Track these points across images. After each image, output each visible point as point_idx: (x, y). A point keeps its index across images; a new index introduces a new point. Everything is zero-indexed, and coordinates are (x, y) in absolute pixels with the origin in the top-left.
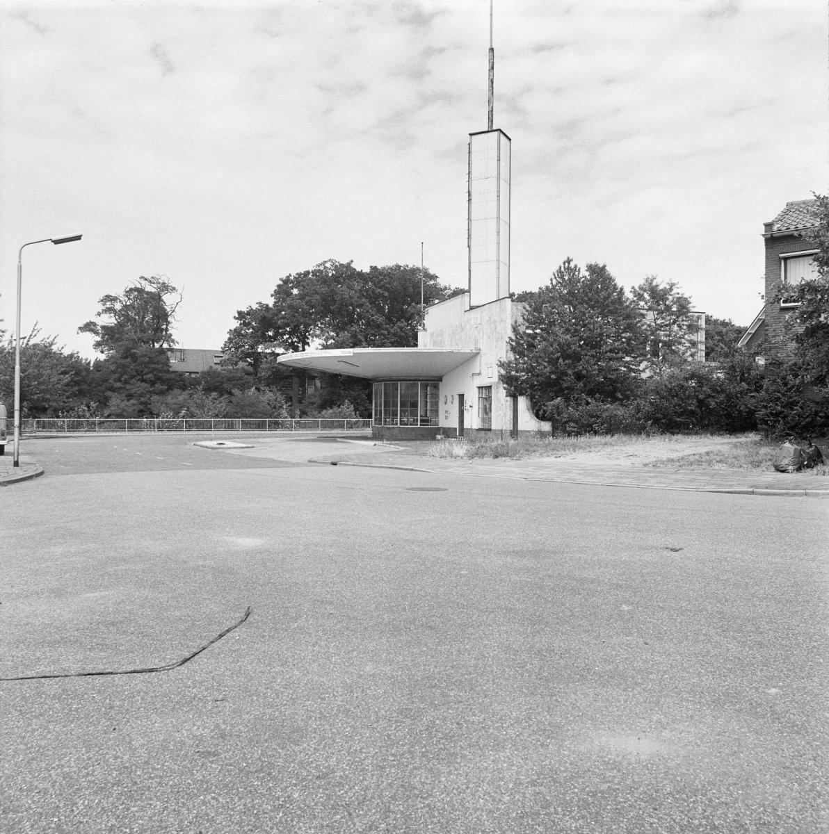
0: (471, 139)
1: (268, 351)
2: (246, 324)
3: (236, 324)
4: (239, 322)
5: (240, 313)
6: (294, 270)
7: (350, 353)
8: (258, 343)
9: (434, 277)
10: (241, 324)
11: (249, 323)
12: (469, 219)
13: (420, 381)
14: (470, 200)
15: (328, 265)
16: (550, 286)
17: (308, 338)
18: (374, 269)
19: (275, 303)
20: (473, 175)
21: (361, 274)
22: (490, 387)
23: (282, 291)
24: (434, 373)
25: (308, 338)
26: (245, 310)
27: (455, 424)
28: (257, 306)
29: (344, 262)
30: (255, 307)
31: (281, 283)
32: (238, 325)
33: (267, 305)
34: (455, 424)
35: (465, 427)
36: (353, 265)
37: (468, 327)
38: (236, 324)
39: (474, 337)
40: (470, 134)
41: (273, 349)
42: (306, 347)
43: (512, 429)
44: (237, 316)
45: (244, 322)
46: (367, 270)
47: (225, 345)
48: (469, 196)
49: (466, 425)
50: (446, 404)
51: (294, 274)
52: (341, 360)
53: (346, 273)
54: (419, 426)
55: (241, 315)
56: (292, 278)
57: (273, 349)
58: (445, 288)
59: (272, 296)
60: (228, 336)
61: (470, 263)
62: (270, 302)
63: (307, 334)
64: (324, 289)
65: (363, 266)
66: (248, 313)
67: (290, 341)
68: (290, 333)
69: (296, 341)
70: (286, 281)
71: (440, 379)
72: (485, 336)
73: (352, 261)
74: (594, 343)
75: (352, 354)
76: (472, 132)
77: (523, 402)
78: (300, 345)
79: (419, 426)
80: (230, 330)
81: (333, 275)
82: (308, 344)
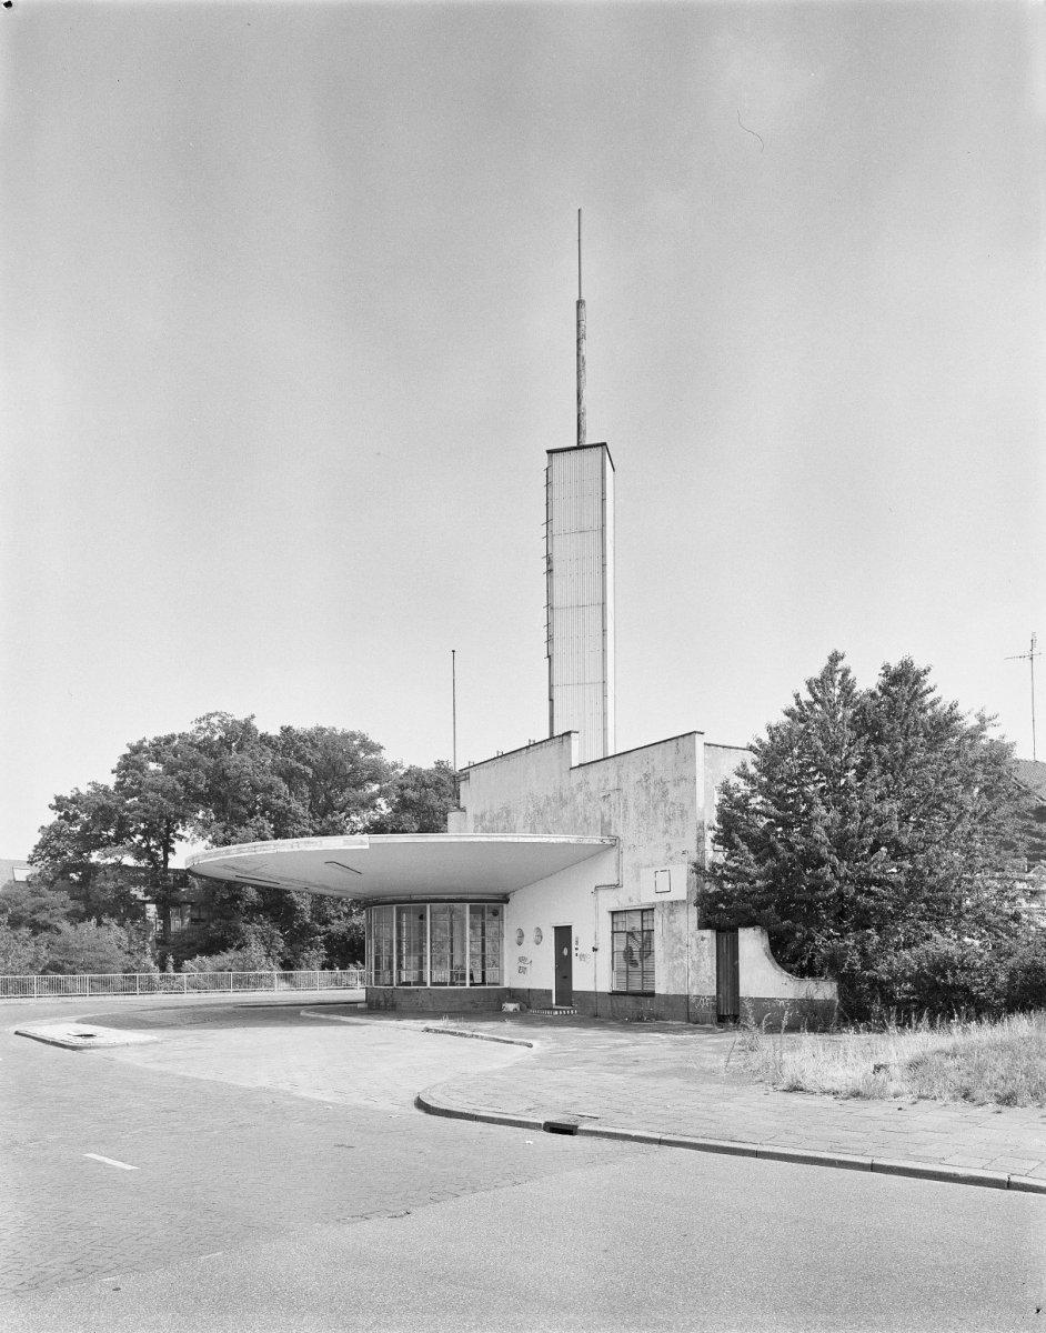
0: (550, 459)
1: (110, 861)
2: (70, 819)
3: (51, 818)
4: (58, 813)
5: (58, 799)
6: (152, 732)
7: (362, 843)
8: (90, 849)
9: (377, 749)
10: (60, 818)
11: (76, 816)
12: (550, 607)
13: (428, 901)
14: (550, 571)
15: (215, 720)
16: (797, 708)
17: (173, 842)
18: (287, 730)
19: (117, 783)
20: (556, 526)
21: (266, 740)
22: (653, 909)
23: (130, 764)
24: (501, 890)
25: (173, 842)
26: (69, 795)
27: (542, 977)
28: (90, 788)
29: (241, 717)
30: (85, 790)
31: (128, 751)
32: (55, 818)
33: (107, 787)
34: (542, 977)
35: (576, 986)
36: (254, 722)
37: (580, 798)
38: (51, 818)
39: (598, 816)
40: (548, 452)
41: (119, 857)
42: (170, 855)
43: (715, 994)
44: (54, 803)
45: (66, 813)
46: (275, 732)
47: (35, 851)
48: (548, 564)
49: (579, 984)
50: (520, 944)
51: (150, 738)
52: (334, 862)
53: (241, 735)
54: (468, 986)
55: (59, 804)
56: (146, 744)
57: (119, 857)
58: (395, 766)
59: (113, 772)
60: (40, 836)
61: (551, 686)
62: (111, 781)
63: (171, 834)
64: (210, 762)
65: (268, 726)
66: (74, 801)
67: (144, 845)
68: (144, 833)
69: (153, 846)
70: (136, 750)
71: (505, 899)
72: (632, 813)
73: (253, 717)
74: (717, 837)
75: (367, 847)
76: (551, 448)
77: (752, 944)
78: (159, 852)
79: (468, 986)
80: (42, 827)
81: (221, 738)
82: (173, 850)
